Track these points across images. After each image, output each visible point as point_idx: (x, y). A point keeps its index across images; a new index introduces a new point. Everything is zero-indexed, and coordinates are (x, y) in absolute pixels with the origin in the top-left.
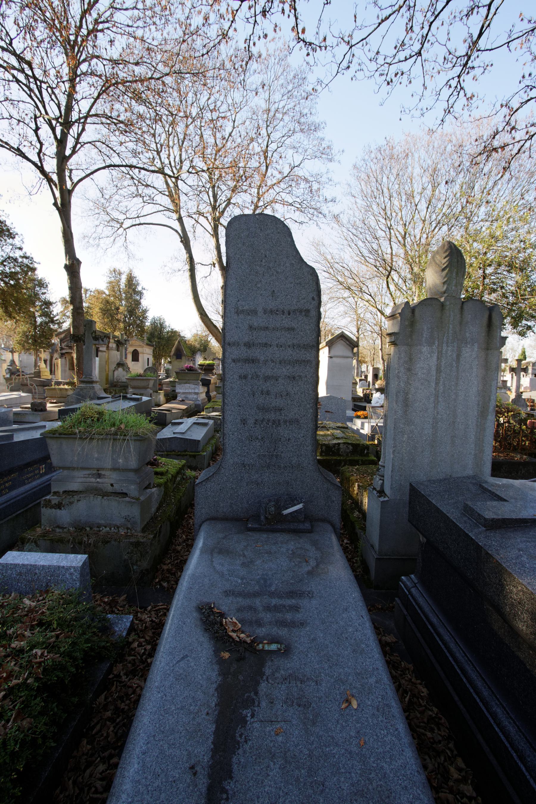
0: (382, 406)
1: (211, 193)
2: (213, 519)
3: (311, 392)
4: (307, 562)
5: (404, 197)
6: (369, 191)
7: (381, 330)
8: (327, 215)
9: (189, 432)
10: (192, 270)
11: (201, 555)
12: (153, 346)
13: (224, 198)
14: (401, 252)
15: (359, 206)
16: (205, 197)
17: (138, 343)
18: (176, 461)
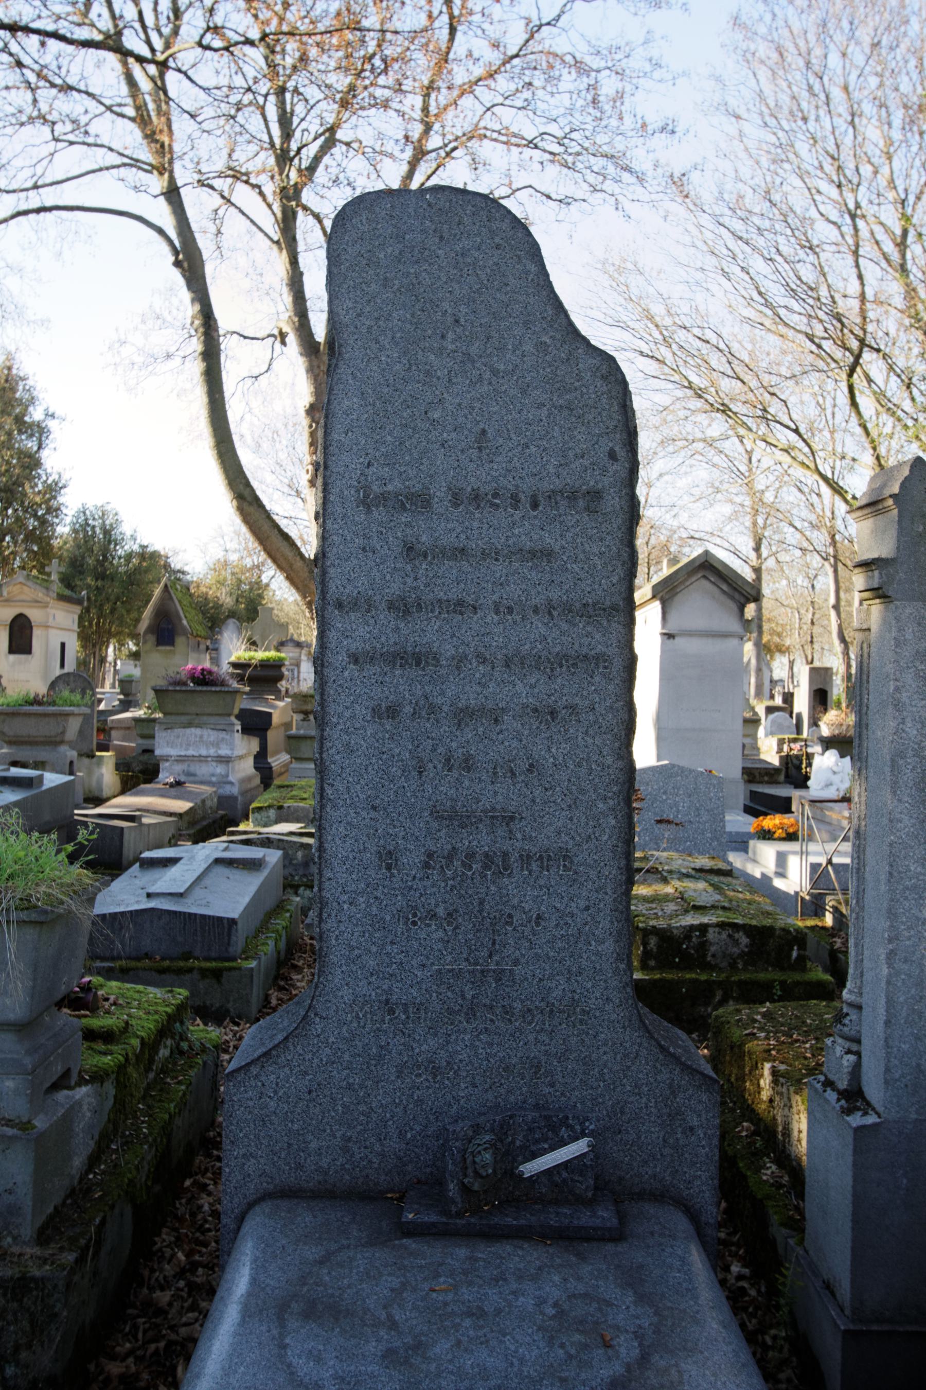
0: (846, 799)
1: (272, 112)
2: (285, 1194)
3: (609, 760)
4: (607, 1345)
5: (898, 116)
6: (785, 99)
7: (834, 542)
8: (650, 173)
9: (198, 892)
10: (211, 355)
11: (243, 1322)
12: (79, 602)
13: (314, 126)
14: (895, 289)
15: (751, 145)
16: (254, 123)
17: (32, 592)
18: (155, 993)
